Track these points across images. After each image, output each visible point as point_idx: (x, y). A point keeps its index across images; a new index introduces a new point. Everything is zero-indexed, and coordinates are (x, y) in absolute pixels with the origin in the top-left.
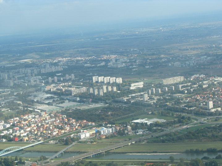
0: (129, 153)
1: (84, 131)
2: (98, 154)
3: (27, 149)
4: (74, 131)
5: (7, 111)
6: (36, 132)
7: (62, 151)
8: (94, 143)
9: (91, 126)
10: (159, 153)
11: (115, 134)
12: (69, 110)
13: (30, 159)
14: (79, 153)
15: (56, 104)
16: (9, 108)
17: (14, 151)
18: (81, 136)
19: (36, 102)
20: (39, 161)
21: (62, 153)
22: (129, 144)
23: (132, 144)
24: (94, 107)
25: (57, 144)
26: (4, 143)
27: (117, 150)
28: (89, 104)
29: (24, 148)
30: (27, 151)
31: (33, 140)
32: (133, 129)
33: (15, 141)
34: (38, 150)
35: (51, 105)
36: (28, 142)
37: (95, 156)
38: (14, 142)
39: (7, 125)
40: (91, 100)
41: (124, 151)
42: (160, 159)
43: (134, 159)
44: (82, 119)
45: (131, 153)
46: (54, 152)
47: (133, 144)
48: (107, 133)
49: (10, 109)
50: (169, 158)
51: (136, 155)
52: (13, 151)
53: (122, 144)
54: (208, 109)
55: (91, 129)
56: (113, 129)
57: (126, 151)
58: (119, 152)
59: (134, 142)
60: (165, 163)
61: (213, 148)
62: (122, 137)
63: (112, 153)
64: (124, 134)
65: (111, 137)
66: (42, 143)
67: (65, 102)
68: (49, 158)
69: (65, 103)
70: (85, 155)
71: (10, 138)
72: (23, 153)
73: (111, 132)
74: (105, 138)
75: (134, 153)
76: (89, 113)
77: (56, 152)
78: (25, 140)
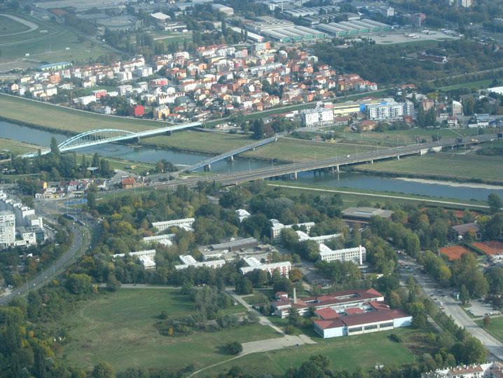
0: (404, 176)
1: (326, 104)
2: (322, 170)
3: (147, 141)
4: (309, 101)
5: (178, 33)
6: (202, 97)
7: (231, 154)
8: (333, 141)
9: (364, 92)
10: (488, 183)
11: (408, 120)
12: (342, 43)
13: (133, 167)
14: (276, 162)
15: (321, 22)
16: (186, 23)
17: (110, 141)
18: (307, 118)
19: (269, 13)
20: (151, 172)
21: (228, 160)
22: (423, 152)
23: (431, 153)
24: (421, 39)
25: (235, 133)
26: (108, 118)
27: (379, 164)
28: (414, 29)
29: (142, 138)
30: (154, 147)
31: (179, 116)
32: (467, 111)
33: (134, 116)
34: (176, 145)
35: (305, 26)
36: (165, 121)
37: (312, 175)
38: (132, 118)
39: (146, 70)
40: (423, 16)
41: (392, 170)
42: (472, 200)
43: (402, 194)
44: (350, 70)
45: (411, 176)
46: (201, 153)
47: (434, 152)
48: (388, 115)
49: (188, 28)
50: (486, 199)
51: (420, 183)
52: (107, 141)
53: (398, 152)
54: (168, 75)
55: (355, 101)
56: (406, 105)
57: (399, 171)
58: (379, 171)
59: (438, 149)
60: (463, 210)
61: (347, 179)
62: (425, 130)
63: (361, 171)
64: (432, 124)
65: (390, 129)
66: (197, 126)
67: (349, 19)
68: (182, 168)
69: (347, 21)
70: (280, 171)
71: (127, 104)
72: (136, 150)
73: (400, 112)
74: (372, 130)
75: (418, 177)
76: (388, 57)
77: (215, 154)
78: (160, 115)
